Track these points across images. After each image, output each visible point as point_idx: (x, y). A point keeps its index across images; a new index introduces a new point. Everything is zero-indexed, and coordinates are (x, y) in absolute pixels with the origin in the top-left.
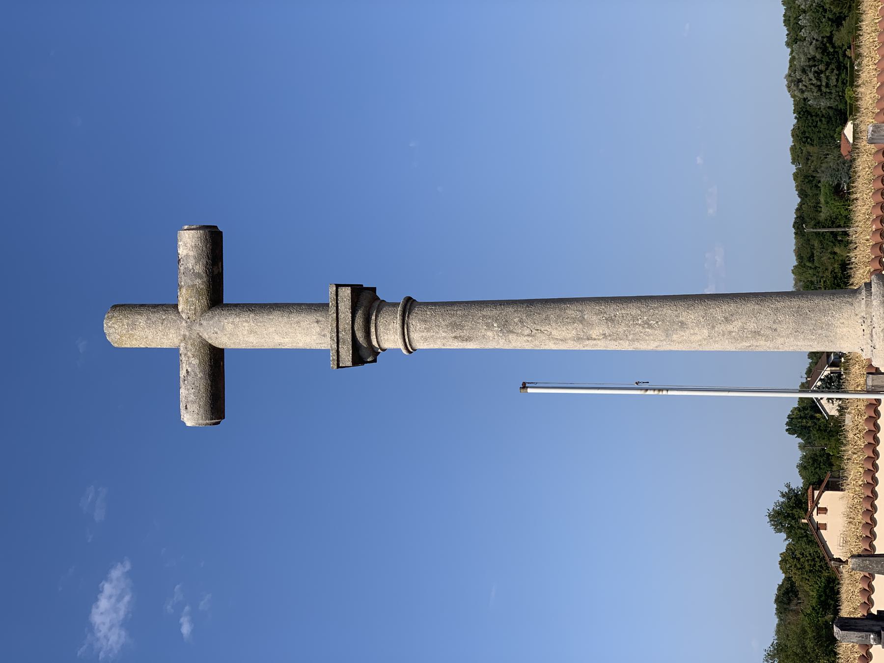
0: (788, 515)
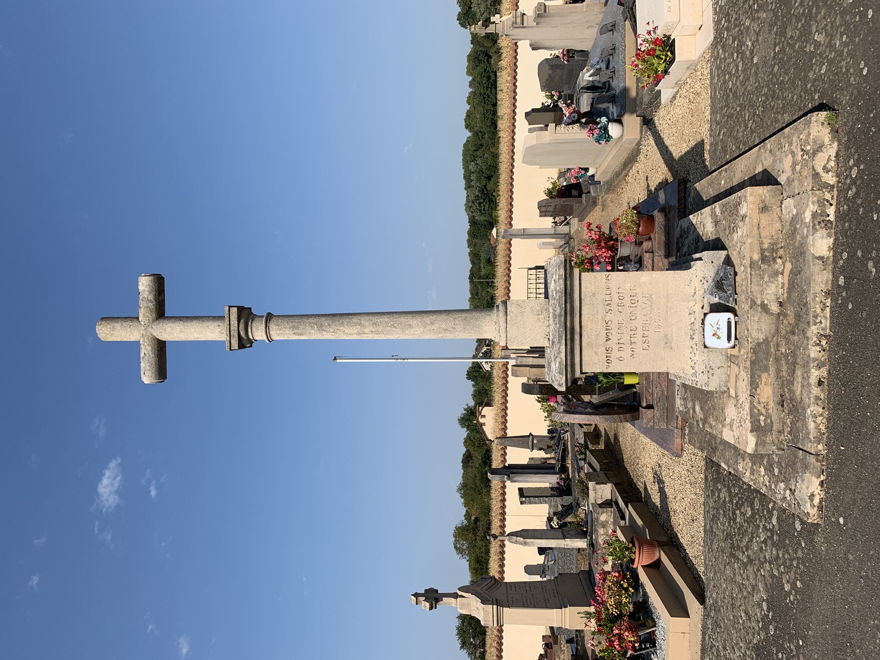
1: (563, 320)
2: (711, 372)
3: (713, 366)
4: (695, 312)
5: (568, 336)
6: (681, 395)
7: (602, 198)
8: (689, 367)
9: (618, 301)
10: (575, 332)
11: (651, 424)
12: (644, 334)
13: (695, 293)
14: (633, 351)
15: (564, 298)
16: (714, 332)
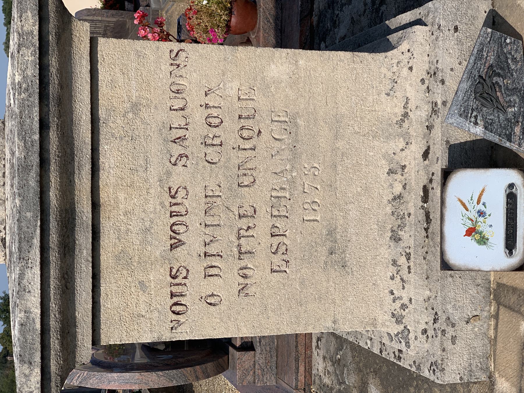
0: (5, 310)
1: (33, 183)
2: (450, 332)
3: (456, 317)
4: (404, 167)
5: (54, 238)
6: (328, 351)
7: (166, 12)
8: (388, 317)
9: (205, 130)
10: (78, 221)
11: (250, 378)
12: (274, 226)
13: (406, 115)
14: (245, 277)
15: (36, 109)
16: (470, 225)
